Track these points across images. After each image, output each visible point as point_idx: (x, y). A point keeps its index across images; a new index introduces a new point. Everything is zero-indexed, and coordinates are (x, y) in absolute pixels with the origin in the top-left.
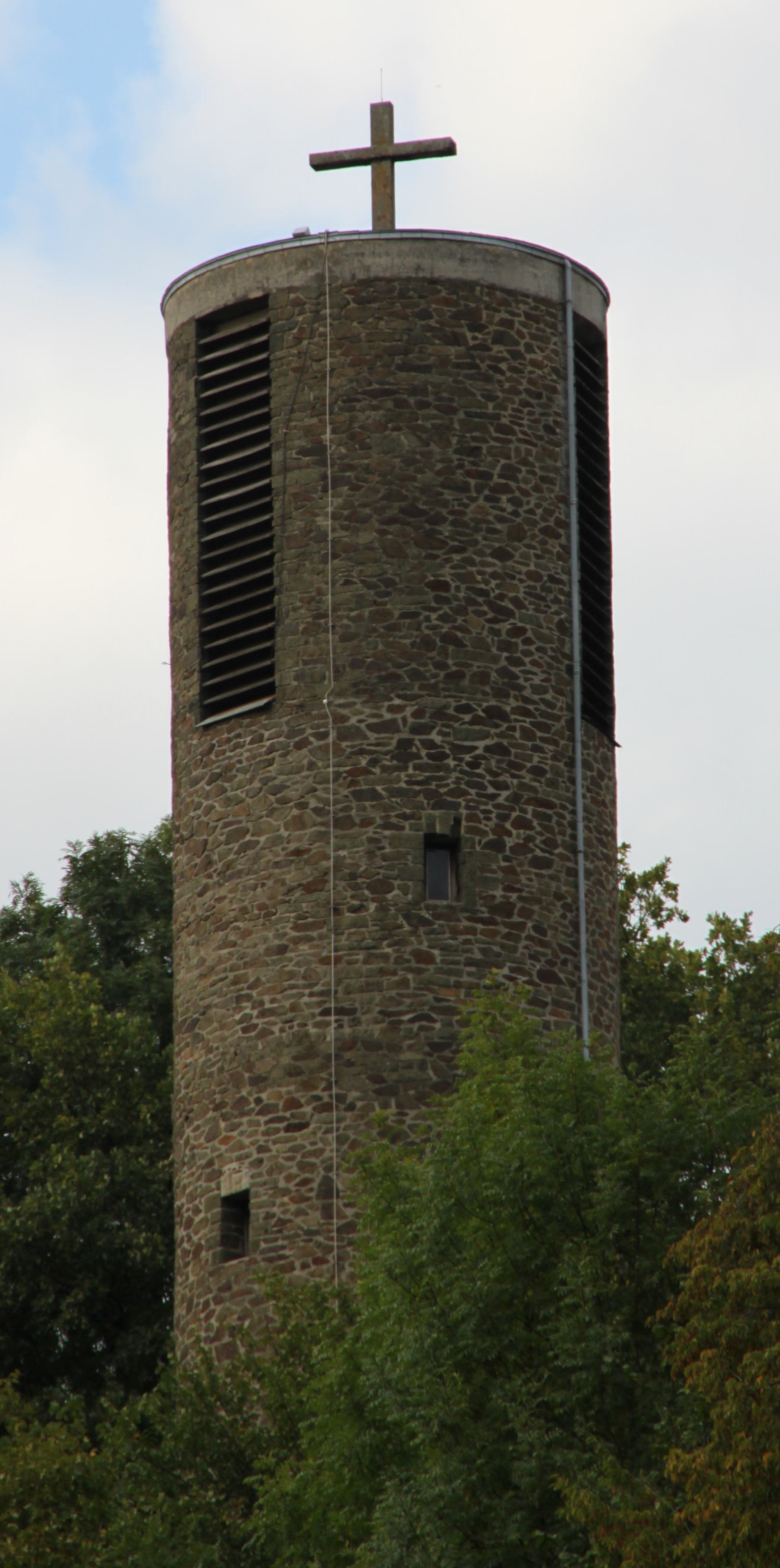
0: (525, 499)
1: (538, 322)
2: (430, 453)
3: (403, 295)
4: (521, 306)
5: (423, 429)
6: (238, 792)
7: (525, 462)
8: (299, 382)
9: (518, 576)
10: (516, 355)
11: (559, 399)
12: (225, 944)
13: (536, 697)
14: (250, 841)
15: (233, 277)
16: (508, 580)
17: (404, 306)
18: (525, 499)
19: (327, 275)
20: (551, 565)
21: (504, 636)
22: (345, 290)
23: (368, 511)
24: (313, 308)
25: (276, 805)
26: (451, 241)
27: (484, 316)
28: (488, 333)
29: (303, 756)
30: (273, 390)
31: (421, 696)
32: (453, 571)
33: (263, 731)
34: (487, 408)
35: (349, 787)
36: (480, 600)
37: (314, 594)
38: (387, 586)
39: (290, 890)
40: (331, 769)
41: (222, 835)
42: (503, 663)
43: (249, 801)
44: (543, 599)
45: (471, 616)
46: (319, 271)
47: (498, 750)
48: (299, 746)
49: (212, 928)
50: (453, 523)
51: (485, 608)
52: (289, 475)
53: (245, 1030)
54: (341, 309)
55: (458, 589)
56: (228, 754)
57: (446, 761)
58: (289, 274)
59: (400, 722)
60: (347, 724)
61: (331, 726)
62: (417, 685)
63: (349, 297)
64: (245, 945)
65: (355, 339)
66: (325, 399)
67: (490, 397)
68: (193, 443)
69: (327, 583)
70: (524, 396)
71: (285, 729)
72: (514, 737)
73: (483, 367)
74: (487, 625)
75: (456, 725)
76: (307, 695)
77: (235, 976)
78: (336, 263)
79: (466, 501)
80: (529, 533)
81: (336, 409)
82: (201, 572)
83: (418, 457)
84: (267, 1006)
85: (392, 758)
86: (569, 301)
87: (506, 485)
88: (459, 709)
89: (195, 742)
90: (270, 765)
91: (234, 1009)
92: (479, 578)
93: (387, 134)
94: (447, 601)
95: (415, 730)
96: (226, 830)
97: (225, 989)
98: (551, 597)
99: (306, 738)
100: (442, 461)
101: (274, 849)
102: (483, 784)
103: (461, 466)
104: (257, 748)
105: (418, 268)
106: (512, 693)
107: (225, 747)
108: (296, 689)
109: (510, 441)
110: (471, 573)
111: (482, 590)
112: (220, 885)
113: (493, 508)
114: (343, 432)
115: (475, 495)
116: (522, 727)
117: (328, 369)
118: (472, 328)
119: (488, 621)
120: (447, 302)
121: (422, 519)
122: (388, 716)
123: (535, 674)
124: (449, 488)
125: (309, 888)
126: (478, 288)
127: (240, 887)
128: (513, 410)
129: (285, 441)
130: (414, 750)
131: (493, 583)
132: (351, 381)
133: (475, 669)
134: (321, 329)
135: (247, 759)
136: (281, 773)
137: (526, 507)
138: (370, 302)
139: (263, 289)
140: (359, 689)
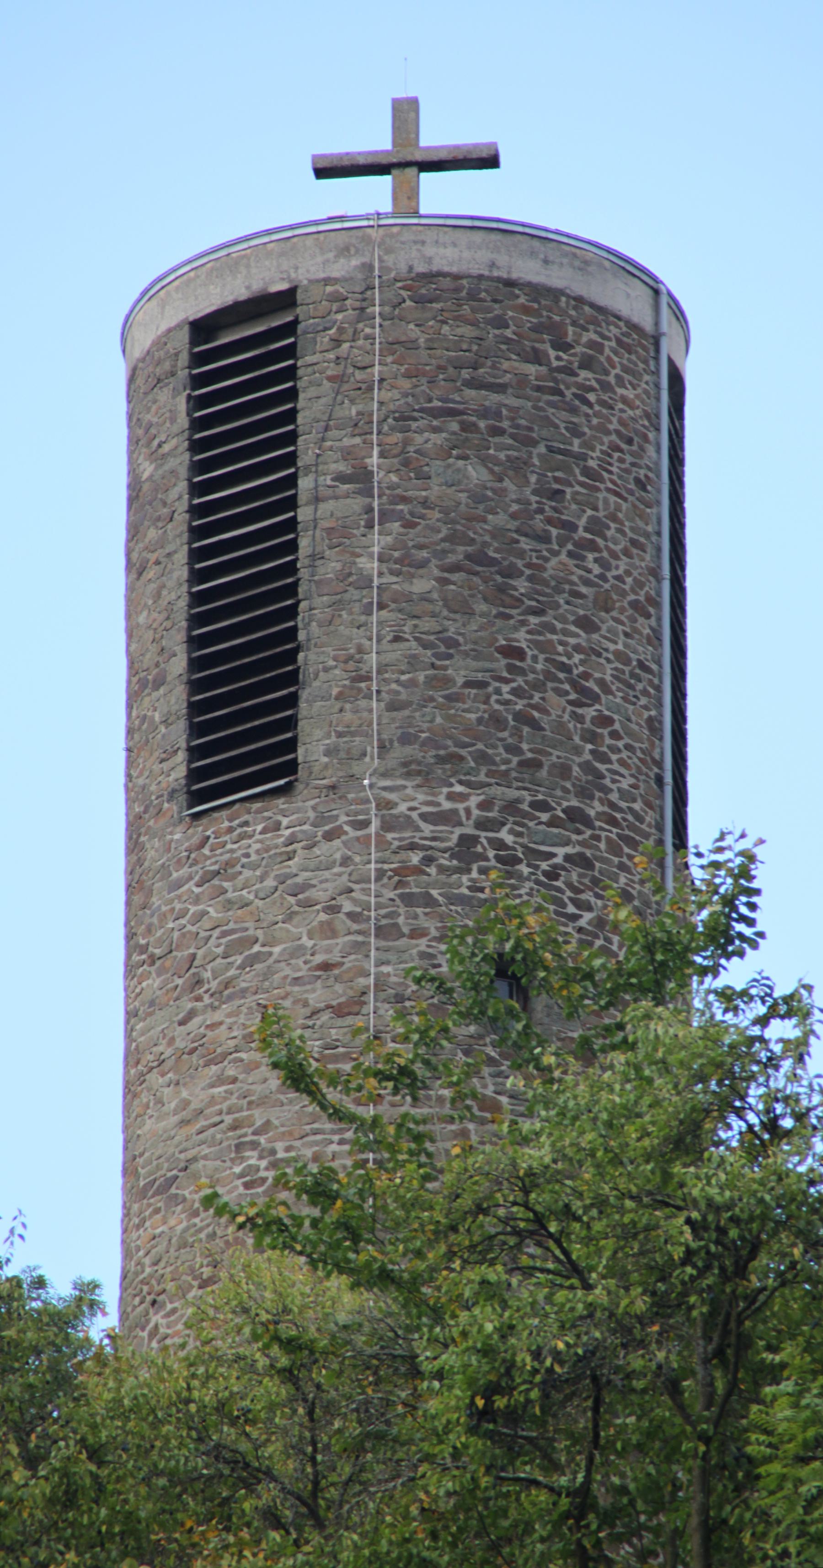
0: (614, 563)
1: (630, 353)
2: (505, 490)
3: (473, 296)
4: (612, 328)
5: (498, 462)
6: (244, 892)
7: (614, 518)
8: (337, 393)
9: (605, 654)
10: (606, 387)
11: (651, 450)
12: (220, 1080)
13: (623, 805)
14: (259, 953)
15: (248, 266)
16: (594, 657)
17: (474, 310)
18: (614, 563)
19: (377, 265)
20: (641, 649)
21: (588, 724)
22: (399, 284)
23: (424, 554)
24: (358, 304)
25: (296, 908)
26: (533, 236)
27: (570, 333)
28: (574, 355)
29: (336, 849)
30: (301, 403)
31: (489, 785)
32: (529, 637)
33: (280, 818)
34: (571, 444)
35: (395, 888)
36: (562, 675)
37: (352, 651)
38: (448, 647)
39: (315, 1013)
40: (373, 866)
41: (218, 946)
42: (587, 756)
43: (260, 903)
44: (632, 687)
45: (550, 694)
46: (366, 259)
47: (581, 861)
48: (329, 836)
49: (201, 1062)
50: (530, 579)
51: (567, 687)
52: (322, 506)
53: (247, 1186)
54: (394, 307)
55: (535, 658)
56: (229, 846)
57: (518, 867)
58: (326, 262)
59: (463, 814)
60: (394, 812)
61: (373, 812)
62: (484, 770)
63: (404, 294)
64: (250, 1080)
65: (411, 345)
66: (371, 414)
67: (575, 431)
68: (183, 472)
69: (370, 639)
70: (614, 437)
71: (311, 815)
72: (598, 849)
73: (568, 394)
74: (569, 708)
75: (531, 824)
76: (341, 774)
77: (235, 1120)
78: (389, 251)
79: (545, 553)
80: (618, 605)
81: (386, 428)
82: (190, 629)
83: (489, 493)
84: (281, 1155)
85: (452, 857)
86: (664, 334)
87: (592, 541)
88: (536, 805)
89: (177, 837)
90: (289, 859)
91: (232, 1160)
92: (560, 649)
93: (413, 136)
94: (522, 672)
95: (481, 825)
96: (224, 941)
97: (219, 1136)
98: (640, 686)
99: (340, 827)
100: (518, 501)
101: (293, 962)
102: (562, 899)
103: (541, 511)
104: (272, 839)
105: (493, 265)
106: (598, 794)
107: (227, 838)
108: (326, 766)
109: (598, 489)
110: (551, 642)
111: (563, 663)
112: (214, 1008)
113: (577, 566)
114: (395, 456)
115: (556, 547)
116: (607, 837)
117: (377, 378)
118: (557, 346)
119: (570, 703)
120: (526, 310)
121: (493, 569)
122: (447, 805)
123: (623, 776)
124: (526, 535)
125: (340, 1011)
126: (564, 299)
127: (244, 1010)
128: (602, 452)
129: (317, 465)
130: (479, 849)
131: (577, 658)
132: (406, 395)
133: (554, 759)
134: (368, 330)
135: (258, 852)
136: (305, 870)
137: (615, 573)
138: (431, 301)
139: (290, 281)
140: (409, 769)
